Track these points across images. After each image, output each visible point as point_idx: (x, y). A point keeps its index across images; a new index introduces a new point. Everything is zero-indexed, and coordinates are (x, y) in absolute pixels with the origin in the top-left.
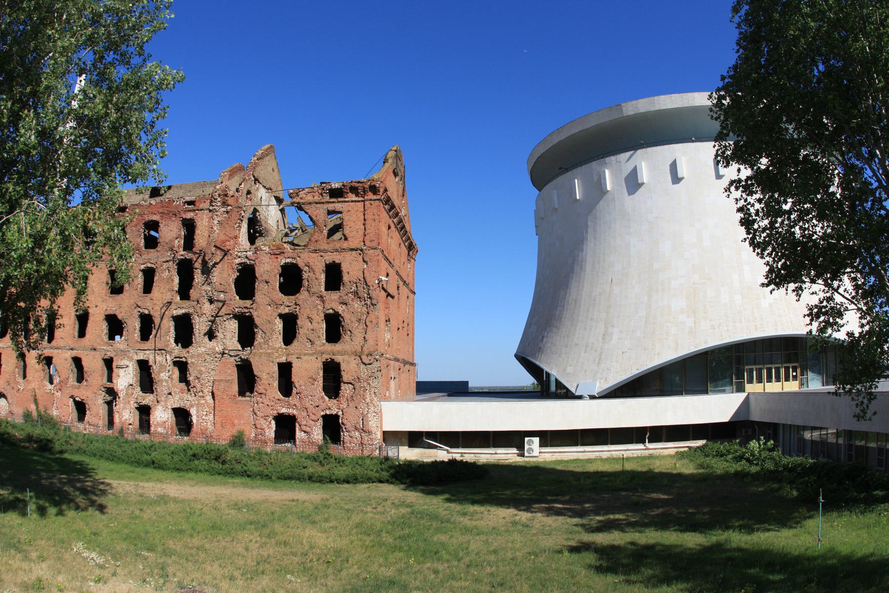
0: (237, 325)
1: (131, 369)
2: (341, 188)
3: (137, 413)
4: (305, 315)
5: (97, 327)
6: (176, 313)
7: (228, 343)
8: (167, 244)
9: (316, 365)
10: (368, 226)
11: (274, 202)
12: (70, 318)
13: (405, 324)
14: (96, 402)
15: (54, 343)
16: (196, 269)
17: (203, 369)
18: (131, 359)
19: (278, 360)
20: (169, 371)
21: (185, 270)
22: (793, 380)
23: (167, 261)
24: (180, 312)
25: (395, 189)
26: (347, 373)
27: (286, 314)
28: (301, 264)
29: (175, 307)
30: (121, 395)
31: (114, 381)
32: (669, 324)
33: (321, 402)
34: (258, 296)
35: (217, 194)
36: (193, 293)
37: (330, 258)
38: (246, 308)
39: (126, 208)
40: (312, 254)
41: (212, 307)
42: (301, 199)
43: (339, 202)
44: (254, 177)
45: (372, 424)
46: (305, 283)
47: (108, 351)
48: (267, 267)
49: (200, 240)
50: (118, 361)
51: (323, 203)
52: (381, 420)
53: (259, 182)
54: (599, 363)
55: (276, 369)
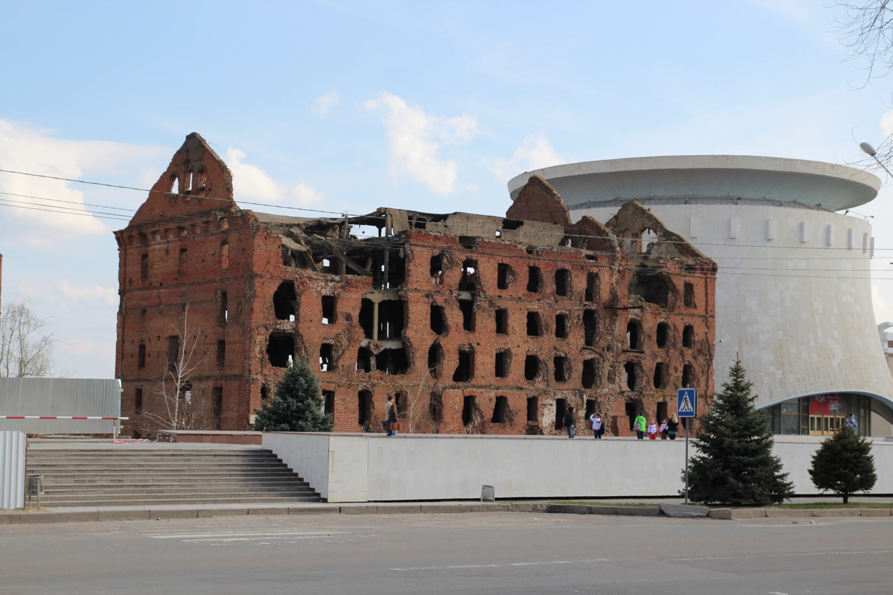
4: (673, 366)
21: (589, 319)
32: (761, 374)
50: (542, 400)
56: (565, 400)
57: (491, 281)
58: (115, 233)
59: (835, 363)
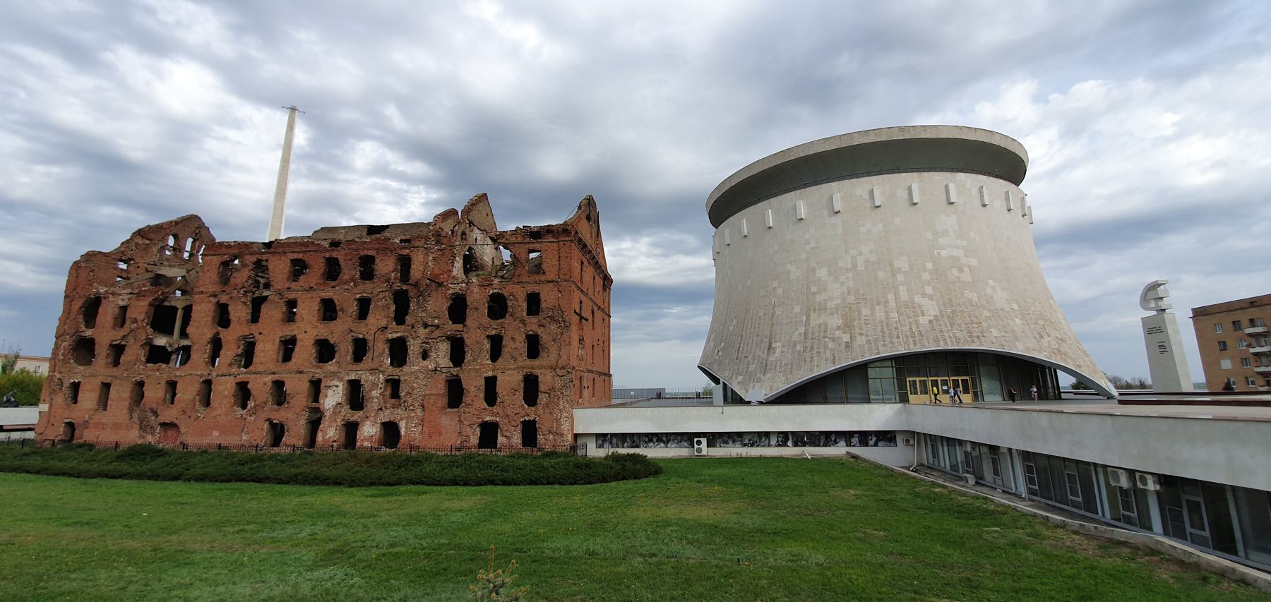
0: (449, 346)
1: (341, 388)
2: (540, 232)
3: (344, 429)
4: (509, 337)
5: (305, 353)
6: (390, 336)
7: (440, 362)
8: (383, 276)
9: (517, 378)
10: (562, 262)
11: (490, 242)
12: (274, 344)
13: (601, 341)
14: (297, 423)
15: (251, 368)
16: (412, 298)
17: (415, 385)
18: (341, 380)
19: (485, 375)
20: (381, 388)
22: (921, 394)
23: (383, 291)
24: (395, 336)
25: (588, 231)
26: (544, 384)
27: (493, 336)
28: (506, 294)
29: (390, 332)
30: (327, 414)
31: (321, 401)
33: (521, 410)
34: (468, 322)
35: (430, 234)
36: (409, 319)
37: (530, 288)
38: (458, 331)
39: (340, 243)
40: (516, 286)
41: (427, 331)
42: (506, 239)
43: (538, 243)
44: (468, 220)
45: (565, 427)
46: (510, 309)
47: (316, 373)
48: (476, 296)
49: (416, 271)
51: (525, 243)
52: (573, 424)
53: (474, 225)
54: (764, 373)
55: (483, 382)
56: (360, 381)
57: (280, 276)
58: (1192, 309)
59: (923, 321)
